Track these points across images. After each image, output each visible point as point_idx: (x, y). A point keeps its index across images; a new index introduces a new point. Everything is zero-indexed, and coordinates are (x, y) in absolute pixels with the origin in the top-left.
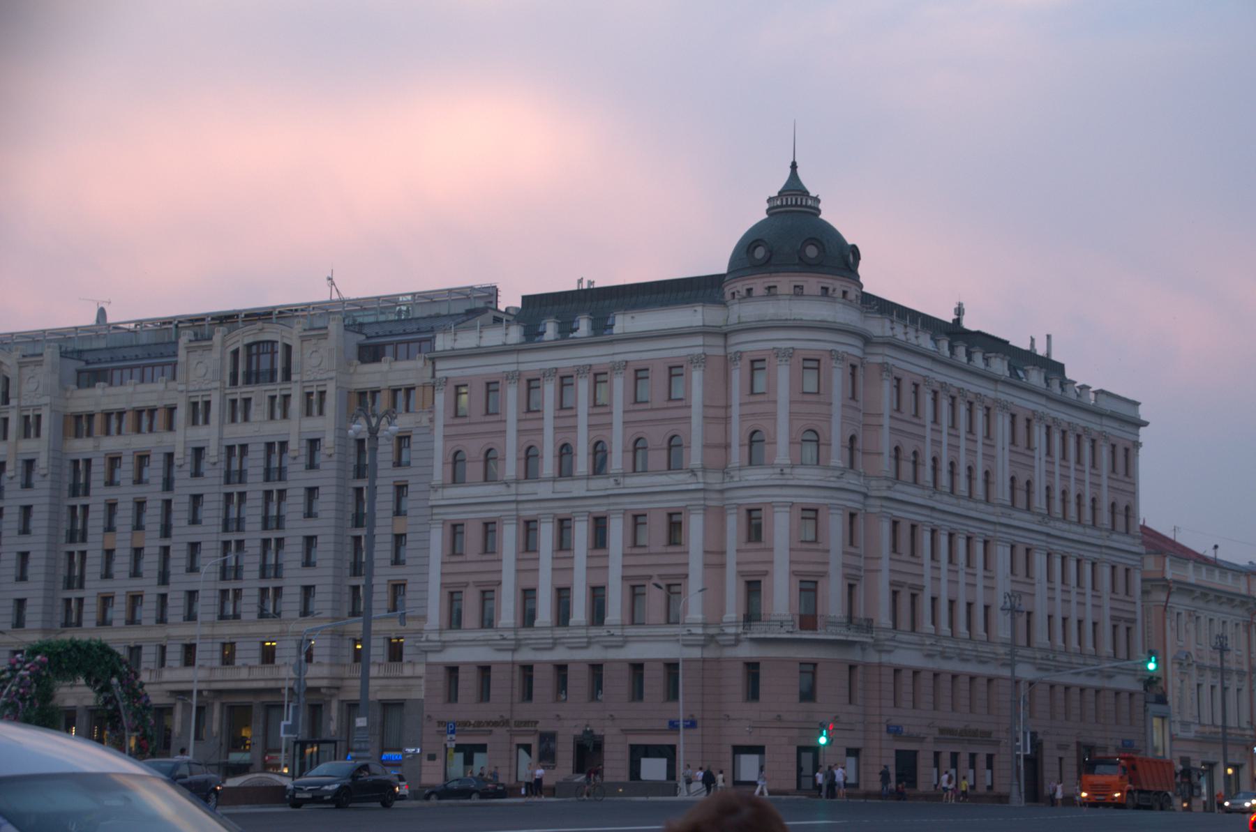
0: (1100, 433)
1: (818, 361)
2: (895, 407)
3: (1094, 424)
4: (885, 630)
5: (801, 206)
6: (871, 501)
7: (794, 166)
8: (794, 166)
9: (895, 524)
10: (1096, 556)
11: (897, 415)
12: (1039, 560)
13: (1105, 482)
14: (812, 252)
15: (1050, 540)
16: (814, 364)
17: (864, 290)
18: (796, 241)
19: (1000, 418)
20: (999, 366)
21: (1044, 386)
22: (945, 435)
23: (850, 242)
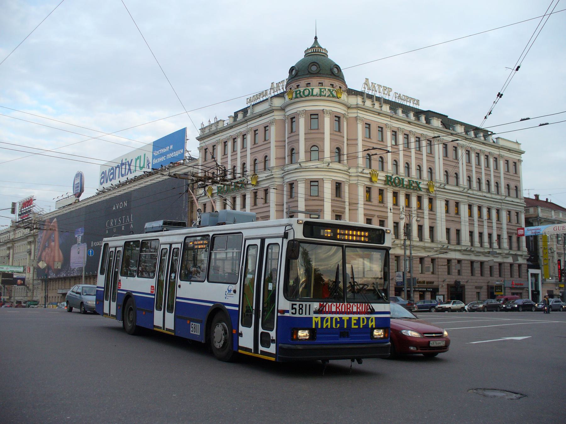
0: (499, 155)
1: (317, 115)
2: (506, 170)
3: (496, 152)
4: (487, 248)
5: (320, 52)
6: (352, 178)
7: (316, 38)
8: (316, 38)
9: (447, 202)
10: (500, 207)
11: (496, 171)
12: (464, 209)
13: (492, 173)
14: (314, 68)
15: (470, 199)
16: (316, 117)
17: (348, 87)
18: (316, 68)
19: (436, 146)
20: (386, 108)
21: (371, 106)
22: (401, 153)
23: (302, 56)
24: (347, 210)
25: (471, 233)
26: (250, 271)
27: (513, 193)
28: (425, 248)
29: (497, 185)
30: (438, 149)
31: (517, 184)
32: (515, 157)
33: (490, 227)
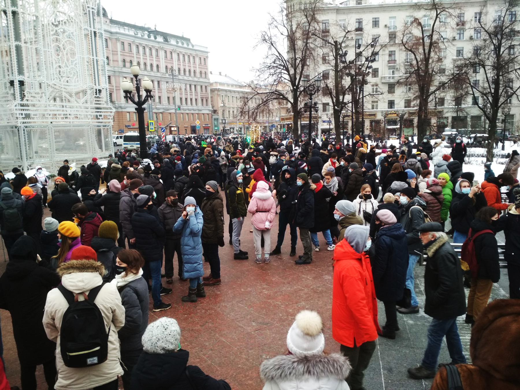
9: (201, 86)
24: (115, 90)
25: (181, 99)
26: (321, 145)
27: (203, 75)
28: (188, 109)
29: (195, 72)
30: (162, 54)
31: (206, 71)
32: (205, 55)
33: (181, 94)
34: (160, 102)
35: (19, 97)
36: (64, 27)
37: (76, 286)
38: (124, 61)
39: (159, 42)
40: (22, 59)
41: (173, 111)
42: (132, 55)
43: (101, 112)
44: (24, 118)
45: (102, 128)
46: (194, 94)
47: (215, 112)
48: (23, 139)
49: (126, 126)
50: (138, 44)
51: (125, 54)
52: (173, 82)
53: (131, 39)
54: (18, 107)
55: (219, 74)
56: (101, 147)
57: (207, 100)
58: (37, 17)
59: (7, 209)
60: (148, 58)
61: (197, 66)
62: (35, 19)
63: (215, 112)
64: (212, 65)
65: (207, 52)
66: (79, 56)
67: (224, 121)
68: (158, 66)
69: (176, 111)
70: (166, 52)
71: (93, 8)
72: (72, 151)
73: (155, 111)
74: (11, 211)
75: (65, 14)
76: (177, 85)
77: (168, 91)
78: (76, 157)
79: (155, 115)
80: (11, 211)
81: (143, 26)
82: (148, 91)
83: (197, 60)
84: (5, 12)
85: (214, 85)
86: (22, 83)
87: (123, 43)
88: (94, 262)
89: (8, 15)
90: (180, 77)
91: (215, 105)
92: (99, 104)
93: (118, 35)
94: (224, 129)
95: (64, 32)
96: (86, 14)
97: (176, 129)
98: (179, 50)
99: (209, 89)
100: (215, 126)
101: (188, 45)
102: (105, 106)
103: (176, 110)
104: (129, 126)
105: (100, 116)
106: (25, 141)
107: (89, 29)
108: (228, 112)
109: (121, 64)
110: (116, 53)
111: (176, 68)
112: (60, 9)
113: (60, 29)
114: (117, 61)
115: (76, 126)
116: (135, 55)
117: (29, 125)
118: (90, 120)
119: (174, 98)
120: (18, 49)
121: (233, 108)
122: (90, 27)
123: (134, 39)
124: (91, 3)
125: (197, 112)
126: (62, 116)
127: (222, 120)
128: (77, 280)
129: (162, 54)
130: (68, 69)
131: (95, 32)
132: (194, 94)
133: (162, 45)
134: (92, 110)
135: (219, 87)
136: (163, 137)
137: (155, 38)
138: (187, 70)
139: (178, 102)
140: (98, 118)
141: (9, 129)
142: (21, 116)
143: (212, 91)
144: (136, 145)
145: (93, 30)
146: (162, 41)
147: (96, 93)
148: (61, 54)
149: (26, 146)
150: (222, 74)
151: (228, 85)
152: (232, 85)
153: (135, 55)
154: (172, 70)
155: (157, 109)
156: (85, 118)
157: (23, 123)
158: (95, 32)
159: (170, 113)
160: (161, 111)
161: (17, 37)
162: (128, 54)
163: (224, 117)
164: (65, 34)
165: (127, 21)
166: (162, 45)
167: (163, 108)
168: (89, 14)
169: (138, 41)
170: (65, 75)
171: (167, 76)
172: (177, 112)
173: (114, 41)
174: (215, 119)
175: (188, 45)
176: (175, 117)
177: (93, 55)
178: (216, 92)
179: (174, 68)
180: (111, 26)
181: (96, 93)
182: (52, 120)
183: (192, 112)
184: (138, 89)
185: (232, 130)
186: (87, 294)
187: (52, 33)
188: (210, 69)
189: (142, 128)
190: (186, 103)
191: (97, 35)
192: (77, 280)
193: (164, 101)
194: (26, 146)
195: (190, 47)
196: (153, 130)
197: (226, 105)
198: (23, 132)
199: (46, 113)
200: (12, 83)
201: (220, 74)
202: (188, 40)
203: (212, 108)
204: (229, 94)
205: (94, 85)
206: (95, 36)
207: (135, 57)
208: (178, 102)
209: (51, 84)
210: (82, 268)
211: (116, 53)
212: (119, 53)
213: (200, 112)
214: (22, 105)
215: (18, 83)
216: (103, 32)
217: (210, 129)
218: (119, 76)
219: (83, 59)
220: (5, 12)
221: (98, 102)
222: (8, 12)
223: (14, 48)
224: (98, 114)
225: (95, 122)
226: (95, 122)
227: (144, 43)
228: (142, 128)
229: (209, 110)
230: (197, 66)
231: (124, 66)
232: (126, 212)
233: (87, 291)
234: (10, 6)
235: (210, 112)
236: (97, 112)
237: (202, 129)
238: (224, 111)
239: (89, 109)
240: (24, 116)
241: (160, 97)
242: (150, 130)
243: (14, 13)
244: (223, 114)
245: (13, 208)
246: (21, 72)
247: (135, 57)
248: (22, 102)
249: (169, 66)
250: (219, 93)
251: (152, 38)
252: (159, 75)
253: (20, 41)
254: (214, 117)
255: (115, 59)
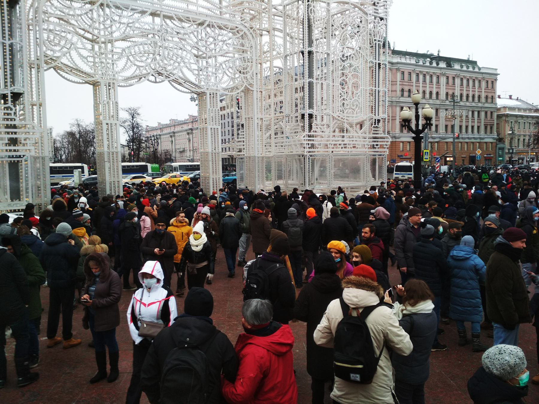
27: (489, 100)
28: (468, 138)
30: (443, 80)
32: (493, 77)
34: (437, 131)
35: (308, 129)
36: (351, 62)
37: (351, 300)
38: (403, 90)
39: (441, 68)
40: (313, 94)
41: (451, 140)
42: (412, 84)
43: (378, 141)
44: (310, 148)
45: (377, 157)
46: (476, 121)
47: (501, 140)
48: (308, 167)
49: (398, 156)
50: (418, 72)
51: (404, 83)
52: (454, 109)
53: (411, 68)
54: (306, 138)
55: (509, 97)
56: (374, 176)
57: (491, 128)
58: (328, 55)
59: (292, 227)
60: (428, 86)
61: (483, 90)
62: (326, 56)
63: (501, 140)
64: (501, 88)
65: (497, 75)
66: (362, 88)
67: (511, 151)
68: (437, 94)
69: (454, 140)
70: (448, 78)
71: (379, 41)
72: (347, 179)
73: (430, 140)
74: (295, 229)
75: (353, 49)
76: (457, 112)
77: (447, 119)
78: (351, 185)
79: (430, 144)
80: (295, 229)
81: (426, 53)
82: (428, 119)
83: (484, 84)
84: (303, 53)
85: (502, 110)
86: (311, 116)
87: (403, 73)
88: (371, 281)
89: (305, 55)
90: (462, 104)
91: (502, 132)
92: (377, 134)
93: (398, 65)
94: (510, 160)
95: (351, 66)
96: (372, 47)
97: (452, 159)
98: (462, 74)
99: (495, 115)
100: (500, 156)
101: (474, 68)
102: (383, 135)
103: (454, 138)
104: (401, 156)
105: (377, 145)
106: (309, 168)
107: (374, 61)
108: (516, 140)
109: (399, 93)
110: (395, 83)
111: (457, 93)
112: (349, 45)
113: (347, 64)
114: (396, 91)
115: (354, 155)
116: (414, 84)
117: (314, 154)
118: (367, 150)
119: (453, 127)
120: (311, 84)
121: (524, 136)
122: (375, 59)
123: (415, 67)
124: (378, 36)
125: (478, 141)
126: (343, 146)
127: (509, 149)
128: (353, 295)
129: (443, 80)
130: (352, 101)
131: (379, 64)
132: (476, 121)
133: (444, 71)
134: (370, 140)
135: (508, 112)
136: (438, 167)
137: (438, 64)
138: (471, 95)
139: (457, 129)
140: (374, 148)
141: (297, 157)
142: (308, 146)
143: (499, 117)
144: (411, 175)
145: (378, 62)
146: (445, 66)
147: (375, 123)
148: (346, 87)
149: (309, 173)
150: (513, 97)
151: (519, 109)
152: (525, 110)
153: (414, 84)
154: (453, 96)
155: (433, 138)
156: (362, 147)
157: (309, 152)
158: (379, 64)
159: (447, 143)
160: (437, 140)
161: (311, 75)
162: (407, 84)
163: (511, 146)
164: (352, 68)
165: (409, 50)
166: (444, 71)
167: (440, 137)
168: (375, 47)
169: (418, 69)
170: (348, 107)
171: (447, 103)
172: (456, 140)
173: (394, 71)
174: (500, 149)
175: (474, 68)
176: (452, 146)
177: (375, 86)
178: (504, 118)
179: (456, 94)
180: (392, 57)
181: (375, 123)
182: (333, 150)
183: (473, 140)
184: (417, 117)
185: (520, 161)
186: (361, 311)
187: (340, 68)
188: (498, 92)
189: (418, 156)
190: (467, 131)
191: (382, 66)
192: (353, 295)
193: (442, 129)
194: (309, 173)
195: (476, 70)
196: (428, 160)
197: (516, 132)
198: (308, 160)
199: (328, 143)
200: (303, 116)
201: (510, 97)
202: (474, 63)
203: (498, 136)
204: (521, 121)
205: (374, 115)
206: (379, 67)
207: (414, 86)
208: (457, 129)
209: (335, 116)
210: (359, 285)
211: (395, 83)
212: (398, 83)
213: (482, 141)
214: (309, 136)
215: (308, 116)
216: (387, 63)
217: (493, 160)
218: (396, 106)
219: (366, 90)
220: (303, 53)
221: (376, 132)
222: (305, 53)
223: (307, 85)
224: (375, 143)
225: (370, 152)
226: (370, 152)
227: (425, 70)
228: (418, 156)
229: (493, 138)
230: (483, 90)
231: (402, 95)
232: (399, 240)
233: (361, 308)
234: (307, 47)
235: (495, 141)
236: (374, 141)
237: (483, 160)
238: (512, 139)
239: (367, 139)
240: (310, 146)
241: (437, 126)
242: (424, 160)
243: (310, 53)
244: (511, 143)
245: (297, 227)
246: (311, 106)
247: (414, 86)
248: (310, 134)
249: (450, 92)
250: (509, 119)
251: (434, 64)
252: (438, 102)
253: (313, 78)
254: (498, 146)
255: (394, 89)
